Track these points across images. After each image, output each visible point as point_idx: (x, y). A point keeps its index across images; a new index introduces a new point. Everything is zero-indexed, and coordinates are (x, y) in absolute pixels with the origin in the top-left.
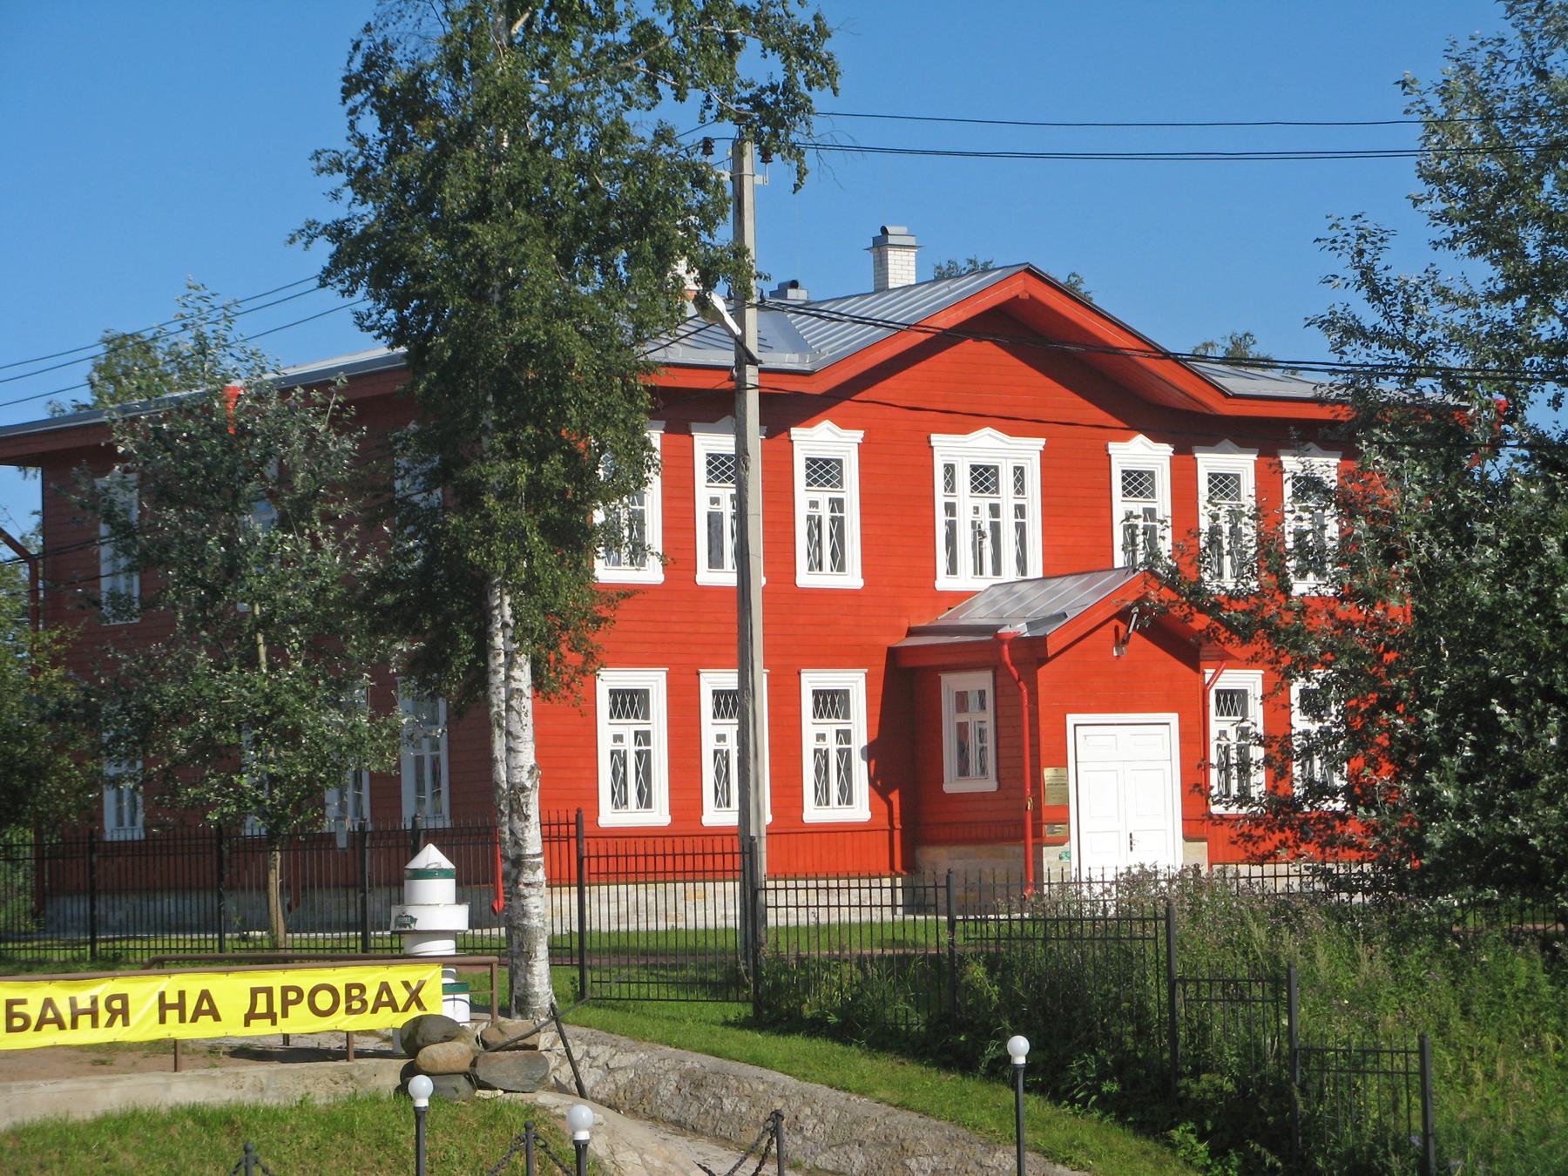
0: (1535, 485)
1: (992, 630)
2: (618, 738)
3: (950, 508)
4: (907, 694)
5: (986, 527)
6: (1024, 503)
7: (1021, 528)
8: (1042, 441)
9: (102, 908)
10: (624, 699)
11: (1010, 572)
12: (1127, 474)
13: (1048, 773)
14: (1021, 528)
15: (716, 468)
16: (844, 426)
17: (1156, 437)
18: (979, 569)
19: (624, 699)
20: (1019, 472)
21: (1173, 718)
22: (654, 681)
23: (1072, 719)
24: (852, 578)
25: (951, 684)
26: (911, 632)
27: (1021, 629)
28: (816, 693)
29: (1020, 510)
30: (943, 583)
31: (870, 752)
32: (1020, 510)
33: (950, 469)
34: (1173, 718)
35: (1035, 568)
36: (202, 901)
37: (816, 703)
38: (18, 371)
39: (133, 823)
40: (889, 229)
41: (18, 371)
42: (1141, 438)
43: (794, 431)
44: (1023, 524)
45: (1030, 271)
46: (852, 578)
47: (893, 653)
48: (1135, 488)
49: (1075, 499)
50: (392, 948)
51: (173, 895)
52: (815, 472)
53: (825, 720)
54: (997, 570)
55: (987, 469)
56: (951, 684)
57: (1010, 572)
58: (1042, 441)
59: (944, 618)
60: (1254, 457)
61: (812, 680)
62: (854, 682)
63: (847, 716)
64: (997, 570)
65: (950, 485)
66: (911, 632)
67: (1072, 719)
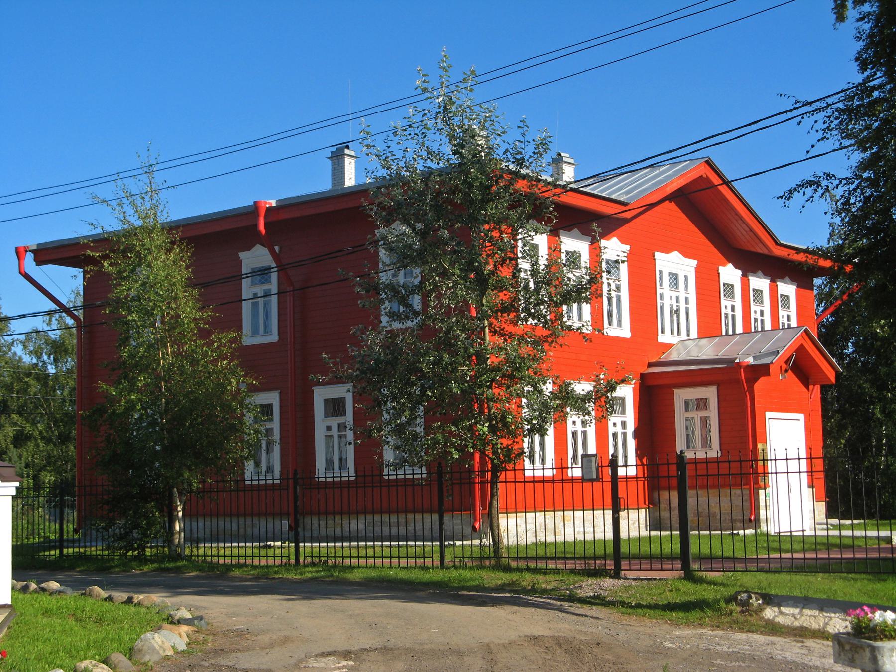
0: (375, 363)
1: (731, 361)
7: (687, 314)
11: (684, 336)
13: (760, 446)
17: (686, 255)
18: (672, 333)
20: (686, 277)
21: (801, 416)
23: (768, 414)
24: (625, 332)
25: (682, 395)
26: (650, 365)
27: (750, 360)
29: (687, 299)
30: (663, 338)
31: (637, 434)
33: (661, 272)
34: (801, 416)
35: (694, 334)
36: (579, 528)
38: (351, 117)
39: (543, 462)
40: (563, 154)
41: (351, 117)
46: (625, 332)
47: (643, 377)
50: (61, 543)
51: (194, 519)
54: (679, 333)
56: (682, 395)
57: (684, 336)
59: (663, 358)
64: (679, 333)
66: (650, 365)
67: (768, 414)
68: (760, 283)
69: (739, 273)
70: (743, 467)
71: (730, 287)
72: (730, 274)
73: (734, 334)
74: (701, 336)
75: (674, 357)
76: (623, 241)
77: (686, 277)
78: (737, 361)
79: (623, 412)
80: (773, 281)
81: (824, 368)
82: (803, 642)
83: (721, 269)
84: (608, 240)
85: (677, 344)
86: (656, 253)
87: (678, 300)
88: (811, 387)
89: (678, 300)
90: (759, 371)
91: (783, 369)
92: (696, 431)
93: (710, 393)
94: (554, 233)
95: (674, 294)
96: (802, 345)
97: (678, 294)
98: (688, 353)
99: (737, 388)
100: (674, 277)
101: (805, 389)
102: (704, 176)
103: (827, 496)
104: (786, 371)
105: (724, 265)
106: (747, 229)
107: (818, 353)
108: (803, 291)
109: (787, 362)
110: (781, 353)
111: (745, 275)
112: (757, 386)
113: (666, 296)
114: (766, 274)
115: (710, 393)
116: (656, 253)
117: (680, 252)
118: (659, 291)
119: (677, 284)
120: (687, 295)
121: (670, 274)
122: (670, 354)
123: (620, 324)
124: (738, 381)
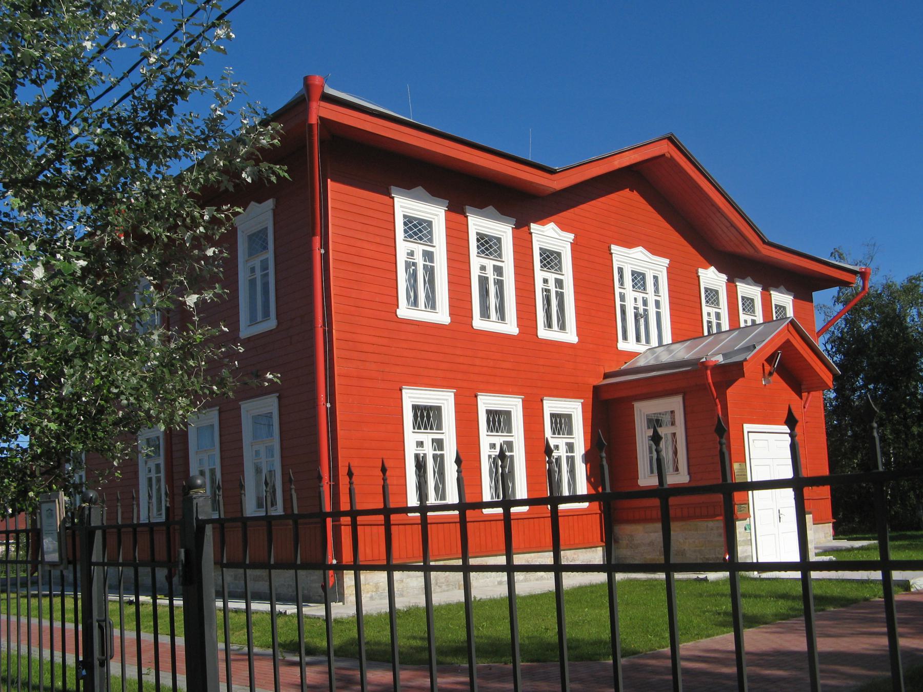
2: (420, 444)
3: (622, 298)
4: (610, 414)
5: (641, 311)
6: (659, 300)
8: (615, 248)
9: (678, 532)
10: (556, 420)
12: (543, 251)
14: (658, 315)
15: (482, 244)
16: (563, 229)
17: (655, 251)
18: (638, 339)
19: (556, 420)
20: (656, 278)
22: (514, 405)
23: (747, 427)
24: (570, 336)
25: (643, 410)
26: (606, 376)
27: (720, 359)
28: (489, 412)
30: (622, 346)
31: (587, 458)
32: (657, 304)
33: (621, 270)
35: (667, 338)
37: (415, 416)
42: (712, 269)
43: (533, 226)
44: (562, 294)
45: (671, 139)
46: (570, 336)
47: (596, 389)
48: (415, 234)
49: (685, 300)
52: (410, 229)
53: (495, 434)
55: (552, 253)
56: (643, 410)
58: (615, 248)
60: (760, 289)
61: (486, 402)
62: (574, 408)
63: (439, 427)
65: (622, 283)
66: (606, 376)
67: (747, 427)
68: (748, 290)
69: (724, 277)
70: (722, 494)
71: (713, 295)
72: (712, 277)
73: (710, 334)
74: (674, 342)
75: (642, 362)
76: (564, 227)
77: (656, 278)
78: (704, 360)
79: (570, 432)
80: (766, 289)
81: (818, 370)
82: (823, 610)
83: (701, 271)
84: (543, 225)
85: (645, 352)
86: (613, 247)
87: (645, 303)
88: (805, 395)
89: (645, 303)
90: (730, 372)
91: (767, 372)
92: (663, 451)
93: (675, 404)
94: (457, 209)
95: (639, 296)
96: (788, 342)
97: (645, 295)
98: (657, 357)
99: (706, 392)
100: (639, 279)
101: (797, 397)
102: (668, 155)
103: (834, 515)
104: (770, 374)
105: (706, 268)
106: (728, 224)
107: (809, 351)
108: (801, 303)
109: (770, 360)
110: (758, 348)
111: (731, 281)
112: (729, 391)
113: (628, 297)
114: (757, 281)
115: (675, 404)
116: (613, 247)
117: (644, 247)
118: (617, 290)
119: (644, 285)
120: (658, 298)
121: (633, 273)
122: (636, 361)
123: (562, 327)
124: (705, 387)
